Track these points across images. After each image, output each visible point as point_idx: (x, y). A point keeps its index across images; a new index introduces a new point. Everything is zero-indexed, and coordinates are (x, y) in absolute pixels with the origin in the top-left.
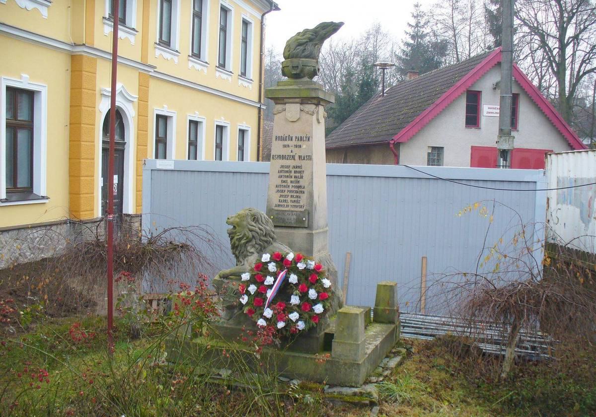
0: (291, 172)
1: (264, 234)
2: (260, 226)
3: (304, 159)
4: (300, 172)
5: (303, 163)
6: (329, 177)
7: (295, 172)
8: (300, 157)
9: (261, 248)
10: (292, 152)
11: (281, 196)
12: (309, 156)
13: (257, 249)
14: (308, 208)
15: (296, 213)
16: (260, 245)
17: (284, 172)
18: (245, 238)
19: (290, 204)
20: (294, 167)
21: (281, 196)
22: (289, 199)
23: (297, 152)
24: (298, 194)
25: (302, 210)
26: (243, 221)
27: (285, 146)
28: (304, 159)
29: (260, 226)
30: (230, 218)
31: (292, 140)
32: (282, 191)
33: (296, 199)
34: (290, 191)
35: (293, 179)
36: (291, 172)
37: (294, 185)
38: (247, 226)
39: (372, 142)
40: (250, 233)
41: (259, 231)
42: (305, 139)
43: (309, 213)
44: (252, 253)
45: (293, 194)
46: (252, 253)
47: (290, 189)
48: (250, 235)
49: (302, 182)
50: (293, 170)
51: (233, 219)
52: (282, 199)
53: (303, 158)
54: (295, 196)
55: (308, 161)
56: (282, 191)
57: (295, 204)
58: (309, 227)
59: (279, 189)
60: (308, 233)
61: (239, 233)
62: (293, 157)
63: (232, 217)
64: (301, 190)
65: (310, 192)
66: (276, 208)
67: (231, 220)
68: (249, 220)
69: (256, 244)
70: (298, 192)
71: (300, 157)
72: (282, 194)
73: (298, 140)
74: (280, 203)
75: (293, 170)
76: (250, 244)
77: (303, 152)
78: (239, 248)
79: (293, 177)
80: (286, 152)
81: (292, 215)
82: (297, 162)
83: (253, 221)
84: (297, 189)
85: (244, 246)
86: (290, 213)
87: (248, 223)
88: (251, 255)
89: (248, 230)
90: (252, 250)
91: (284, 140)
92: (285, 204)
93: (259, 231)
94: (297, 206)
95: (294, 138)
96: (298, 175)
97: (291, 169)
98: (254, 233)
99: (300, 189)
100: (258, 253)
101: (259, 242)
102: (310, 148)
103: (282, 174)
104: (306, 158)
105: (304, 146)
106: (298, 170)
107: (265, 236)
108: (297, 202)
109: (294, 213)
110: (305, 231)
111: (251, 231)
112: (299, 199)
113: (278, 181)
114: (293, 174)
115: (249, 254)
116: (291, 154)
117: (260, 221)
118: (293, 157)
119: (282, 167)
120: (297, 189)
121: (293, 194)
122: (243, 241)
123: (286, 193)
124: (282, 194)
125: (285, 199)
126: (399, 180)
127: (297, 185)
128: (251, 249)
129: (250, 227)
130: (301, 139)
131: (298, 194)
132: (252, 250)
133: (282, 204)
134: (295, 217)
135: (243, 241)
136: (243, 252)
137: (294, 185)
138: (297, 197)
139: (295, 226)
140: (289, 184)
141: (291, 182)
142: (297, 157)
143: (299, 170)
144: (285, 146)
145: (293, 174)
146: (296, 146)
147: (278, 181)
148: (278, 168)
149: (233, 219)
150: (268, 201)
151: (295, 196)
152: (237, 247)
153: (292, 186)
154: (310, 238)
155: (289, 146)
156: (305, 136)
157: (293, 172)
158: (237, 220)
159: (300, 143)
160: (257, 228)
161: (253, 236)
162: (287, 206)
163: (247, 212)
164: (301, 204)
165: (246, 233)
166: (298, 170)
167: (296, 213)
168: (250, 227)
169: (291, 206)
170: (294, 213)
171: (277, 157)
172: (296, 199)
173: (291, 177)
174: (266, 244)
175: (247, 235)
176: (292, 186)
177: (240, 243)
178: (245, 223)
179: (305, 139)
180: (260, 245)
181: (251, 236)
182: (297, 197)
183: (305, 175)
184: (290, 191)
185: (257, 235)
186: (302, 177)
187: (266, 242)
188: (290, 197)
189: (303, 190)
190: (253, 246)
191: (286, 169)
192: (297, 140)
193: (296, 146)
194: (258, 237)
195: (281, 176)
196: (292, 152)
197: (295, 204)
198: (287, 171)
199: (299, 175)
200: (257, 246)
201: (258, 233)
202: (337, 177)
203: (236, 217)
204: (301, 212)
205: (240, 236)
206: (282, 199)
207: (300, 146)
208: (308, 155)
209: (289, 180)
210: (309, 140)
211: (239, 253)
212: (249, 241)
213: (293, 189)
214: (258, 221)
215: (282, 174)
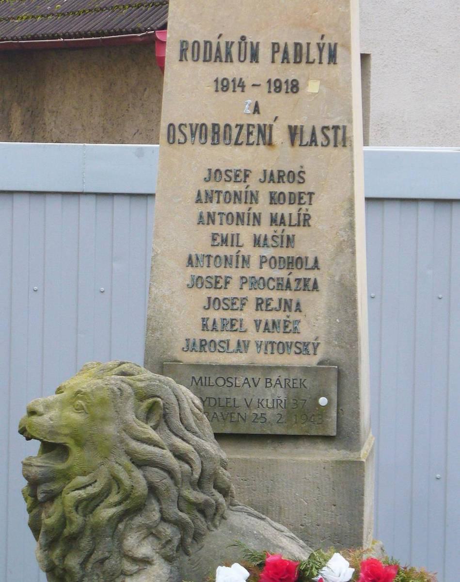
0: (253, 197)
1: (196, 476)
2: (178, 442)
3: (313, 141)
4: (296, 198)
5: (310, 159)
6: (376, 207)
7: (274, 199)
8: (294, 132)
9: (182, 541)
10: (256, 109)
11: (212, 303)
12: (336, 128)
13: (169, 542)
14: (335, 354)
15: (284, 375)
16: (180, 524)
17: (222, 196)
18: (114, 498)
19: (253, 335)
20: (270, 177)
21: (212, 303)
22: (248, 315)
23: (281, 111)
24: (287, 295)
25: (312, 361)
26: (103, 419)
27: (223, 85)
28: (313, 141)
29: (178, 442)
30: (40, 409)
31: (255, 57)
32: (215, 283)
33: (280, 316)
34: (255, 283)
35: (265, 229)
36: (253, 197)
37: (268, 252)
38: (122, 441)
39: (98, 34)
40: (138, 474)
41: (174, 463)
42: (314, 54)
43: (341, 375)
44: (146, 561)
45: (264, 294)
46: (146, 561)
47: (254, 270)
48: (138, 481)
49: (306, 244)
50: (264, 190)
51: (53, 413)
52: (216, 315)
53: (307, 138)
54: (274, 304)
55: (335, 152)
56: (215, 283)
57: (277, 337)
58: (344, 434)
59: (203, 272)
60: (339, 462)
61: (84, 474)
62: (264, 135)
63: (48, 407)
64: (302, 274)
65: (342, 284)
66: (192, 357)
67: (45, 420)
68: (130, 417)
69: (163, 519)
70: (288, 287)
71: (294, 132)
72: (214, 293)
73: (285, 59)
74: (209, 336)
75: (264, 190)
76: (139, 520)
77: (311, 106)
78: (85, 543)
79: (265, 220)
80: (235, 110)
81: (268, 381)
82: (282, 156)
83: (147, 419)
84: (283, 274)
85: (109, 531)
86: (257, 375)
87: (127, 429)
88: (138, 572)
89: (125, 460)
90: (145, 549)
91: (218, 58)
92: (233, 338)
93: (174, 463)
94: (284, 347)
95: (265, 53)
96: (286, 210)
97: (253, 184)
98: (157, 476)
99: (297, 273)
100: (169, 559)
101: (173, 511)
102: (337, 93)
103: (213, 207)
104: (320, 138)
105: (313, 87)
106: (285, 188)
107: (199, 485)
108: (286, 326)
109: (274, 378)
110: (317, 457)
111: (142, 463)
112: (294, 316)
113: (199, 240)
114: (263, 207)
115: (128, 566)
116: (256, 120)
117: (176, 422)
118: (264, 135)
119: (214, 175)
120: (283, 274)
121: (264, 294)
122: (106, 513)
123: (233, 291)
124: (214, 293)
125: (229, 315)
126: (21, 203)
127: (285, 253)
128: (140, 544)
129: (134, 445)
130: (298, 54)
131: (287, 295)
132: (145, 549)
133: (217, 336)
134: (281, 393)
135: (106, 513)
136: (102, 561)
137: (268, 252)
138: (286, 305)
139: (279, 430)
140: (248, 249)
141: (257, 242)
142: (280, 135)
143: (292, 192)
144: (223, 85)
145: (263, 207)
146: (276, 86)
147: (199, 240)
148: (195, 182)
149: (53, 413)
150: (152, 327)
151: (274, 304)
152: (74, 538)
153: (263, 260)
154: (350, 479)
155: (242, 85)
156: (315, 40)
157: (264, 198)
158: (77, 417)
159: (291, 72)
160: (168, 453)
161: (152, 489)
162: (242, 346)
163: (114, 380)
164: (306, 334)
165: (123, 475)
166: (285, 188)
167: (284, 375)
168: (134, 445)
169: (259, 346)
170: (274, 378)
171: (187, 131)
172: (280, 316)
173: (257, 219)
174: (201, 522)
175: (127, 482)
176: (263, 260)
177: (92, 520)
178: (111, 429)
179: (314, 54)
180: (180, 524)
181: (142, 487)
182: (286, 305)
183: (318, 209)
184: (255, 283)
185: (168, 481)
186: (305, 221)
187: (202, 509)
188: (251, 305)
189: (311, 275)
190: (151, 532)
191: (232, 187)
192: (279, 57)
193: (276, 86)
194: (174, 490)
195: (211, 217)
196: (256, 109)
197: (277, 337)
198: (237, 197)
199: (293, 209)
200: (168, 530)
201: (170, 472)
202: (93, 198)
203: (64, 404)
204: (306, 370)
205: (91, 490)
206: (216, 315)
207: (294, 87)
208: (330, 124)
209: (246, 233)
210: (332, 58)
211: (83, 565)
212: (133, 509)
213: (267, 272)
214: (165, 417)
215: (213, 207)
